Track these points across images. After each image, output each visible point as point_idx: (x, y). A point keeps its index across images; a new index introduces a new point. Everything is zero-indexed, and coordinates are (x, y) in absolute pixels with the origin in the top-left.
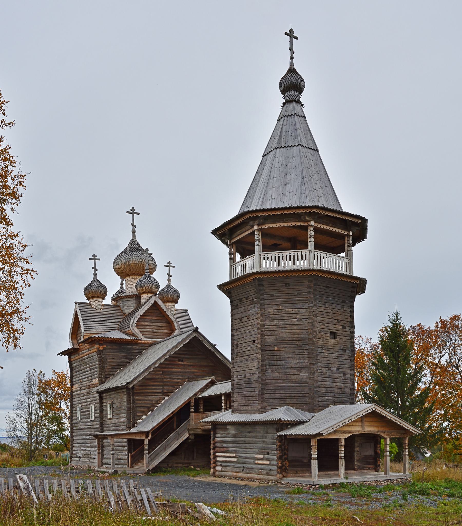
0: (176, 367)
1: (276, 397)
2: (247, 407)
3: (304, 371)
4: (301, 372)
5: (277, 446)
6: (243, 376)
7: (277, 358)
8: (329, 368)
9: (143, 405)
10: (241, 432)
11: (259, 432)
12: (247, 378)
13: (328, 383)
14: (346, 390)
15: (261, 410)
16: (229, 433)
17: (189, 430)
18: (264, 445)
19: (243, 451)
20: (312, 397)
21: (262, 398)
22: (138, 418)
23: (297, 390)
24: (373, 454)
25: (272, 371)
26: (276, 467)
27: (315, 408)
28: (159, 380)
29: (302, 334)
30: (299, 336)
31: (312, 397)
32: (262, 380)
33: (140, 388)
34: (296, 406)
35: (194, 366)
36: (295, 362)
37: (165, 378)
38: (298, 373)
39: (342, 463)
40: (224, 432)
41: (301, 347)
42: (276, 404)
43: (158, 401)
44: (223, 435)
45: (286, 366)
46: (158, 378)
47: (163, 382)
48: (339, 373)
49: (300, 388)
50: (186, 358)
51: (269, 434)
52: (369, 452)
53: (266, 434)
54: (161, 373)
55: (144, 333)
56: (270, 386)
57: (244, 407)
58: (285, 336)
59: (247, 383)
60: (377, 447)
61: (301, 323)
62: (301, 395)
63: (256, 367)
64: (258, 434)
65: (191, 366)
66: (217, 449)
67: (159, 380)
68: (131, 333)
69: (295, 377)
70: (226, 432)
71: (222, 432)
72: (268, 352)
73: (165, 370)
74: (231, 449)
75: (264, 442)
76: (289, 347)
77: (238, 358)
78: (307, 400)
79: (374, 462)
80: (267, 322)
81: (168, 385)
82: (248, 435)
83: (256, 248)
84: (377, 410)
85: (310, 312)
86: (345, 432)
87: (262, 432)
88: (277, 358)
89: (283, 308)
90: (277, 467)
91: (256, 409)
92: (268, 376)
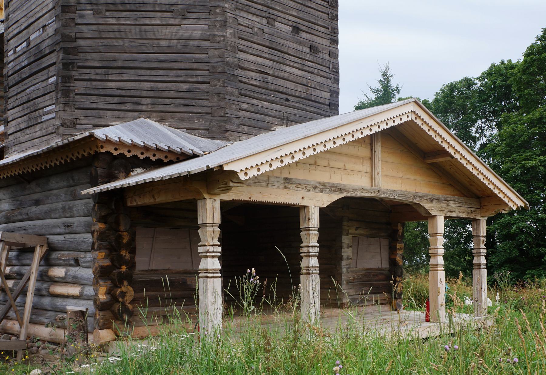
1: (108, 92)
2: (32, 130)
3: (195, 16)
4: (184, 18)
6: (24, 45)
8: (271, 20)
10: (22, 205)
12: (32, 45)
13: (269, 63)
14: (318, 93)
15: (61, 130)
20: (218, 94)
21: (66, 93)
24: (386, 265)
25: (96, 13)
27: (228, 127)
31: (218, 94)
32: (65, 38)
34: (173, 119)
38: (177, 21)
39: (311, 286)
42: (109, 113)
48: (300, 43)
49: (182, 65)
52: (375, 259)
56: (89, 56)
57: (28, 131)
59: (32, 59)
60: (396, 249)
62: (185, 87)
64: (53, 206)
78: (205, 103)
79: (384, 287)
82: (34, 210)
84: (418, 122)
86: (321, 187)
90: (95, 302)
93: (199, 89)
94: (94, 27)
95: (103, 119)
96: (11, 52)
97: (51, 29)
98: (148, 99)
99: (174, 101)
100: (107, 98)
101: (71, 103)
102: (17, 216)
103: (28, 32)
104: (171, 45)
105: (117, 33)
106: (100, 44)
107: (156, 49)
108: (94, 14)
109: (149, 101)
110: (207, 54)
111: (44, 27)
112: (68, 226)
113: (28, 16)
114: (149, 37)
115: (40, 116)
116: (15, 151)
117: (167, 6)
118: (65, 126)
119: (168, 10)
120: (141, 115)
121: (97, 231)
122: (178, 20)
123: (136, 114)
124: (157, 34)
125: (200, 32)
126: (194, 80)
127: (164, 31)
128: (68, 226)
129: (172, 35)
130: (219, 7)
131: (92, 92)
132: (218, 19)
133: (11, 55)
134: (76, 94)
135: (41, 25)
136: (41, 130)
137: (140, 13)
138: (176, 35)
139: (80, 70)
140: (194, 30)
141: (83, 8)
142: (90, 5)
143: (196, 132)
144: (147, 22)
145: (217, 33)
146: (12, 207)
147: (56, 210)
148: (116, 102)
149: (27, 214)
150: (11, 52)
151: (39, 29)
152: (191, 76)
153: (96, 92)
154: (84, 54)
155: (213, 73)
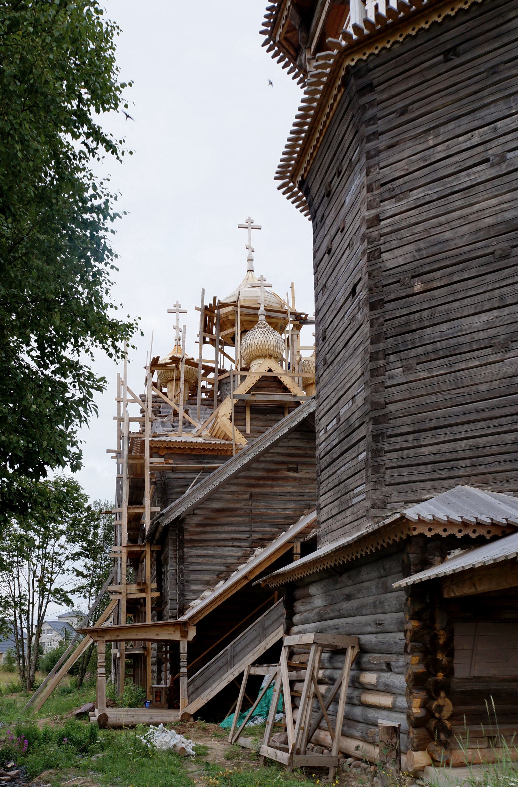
0: (280, 482)
1: (421, 460)
7: (421, 320)
9: (205, 567)
15: (372, 512)
21: (376, 469)
22: (193, 597)
25: (407, 369)
26: (404, 717)
30: (499, 218)
32: (376, 406)
34: (496, 481)
36: (484, 317)
38: (499, 357)
42: (422, 485)
43: (239, 558)
45: (452, 342)
47: (251, 515)
50: (304, 464)
54: (247, 496)
56: (399, 422)
58: (448, 235)
61: (504, 168)
70: (308, 607)
73: (257, 490)
76: (462, 270)
80: (390, 207)
82: (346, 605)
88: (421, 320)
89: (440, 139)
90: (409, 717)
95: (415, 494)
98: (466, 461)
100: (420, 467)
101: (381, 479)
106: (412, 405)
107: (474, 397)
109: (467, 462)
117: (487, 341)
122: (499, 355)
123: (452, 481)
129: (493, 375)
131: (404, 463)
134: (387, 469)
138: (497, 374)
141: (393, 368)
142: (400, 362)
144: (463, 366)
153: (408, 462)
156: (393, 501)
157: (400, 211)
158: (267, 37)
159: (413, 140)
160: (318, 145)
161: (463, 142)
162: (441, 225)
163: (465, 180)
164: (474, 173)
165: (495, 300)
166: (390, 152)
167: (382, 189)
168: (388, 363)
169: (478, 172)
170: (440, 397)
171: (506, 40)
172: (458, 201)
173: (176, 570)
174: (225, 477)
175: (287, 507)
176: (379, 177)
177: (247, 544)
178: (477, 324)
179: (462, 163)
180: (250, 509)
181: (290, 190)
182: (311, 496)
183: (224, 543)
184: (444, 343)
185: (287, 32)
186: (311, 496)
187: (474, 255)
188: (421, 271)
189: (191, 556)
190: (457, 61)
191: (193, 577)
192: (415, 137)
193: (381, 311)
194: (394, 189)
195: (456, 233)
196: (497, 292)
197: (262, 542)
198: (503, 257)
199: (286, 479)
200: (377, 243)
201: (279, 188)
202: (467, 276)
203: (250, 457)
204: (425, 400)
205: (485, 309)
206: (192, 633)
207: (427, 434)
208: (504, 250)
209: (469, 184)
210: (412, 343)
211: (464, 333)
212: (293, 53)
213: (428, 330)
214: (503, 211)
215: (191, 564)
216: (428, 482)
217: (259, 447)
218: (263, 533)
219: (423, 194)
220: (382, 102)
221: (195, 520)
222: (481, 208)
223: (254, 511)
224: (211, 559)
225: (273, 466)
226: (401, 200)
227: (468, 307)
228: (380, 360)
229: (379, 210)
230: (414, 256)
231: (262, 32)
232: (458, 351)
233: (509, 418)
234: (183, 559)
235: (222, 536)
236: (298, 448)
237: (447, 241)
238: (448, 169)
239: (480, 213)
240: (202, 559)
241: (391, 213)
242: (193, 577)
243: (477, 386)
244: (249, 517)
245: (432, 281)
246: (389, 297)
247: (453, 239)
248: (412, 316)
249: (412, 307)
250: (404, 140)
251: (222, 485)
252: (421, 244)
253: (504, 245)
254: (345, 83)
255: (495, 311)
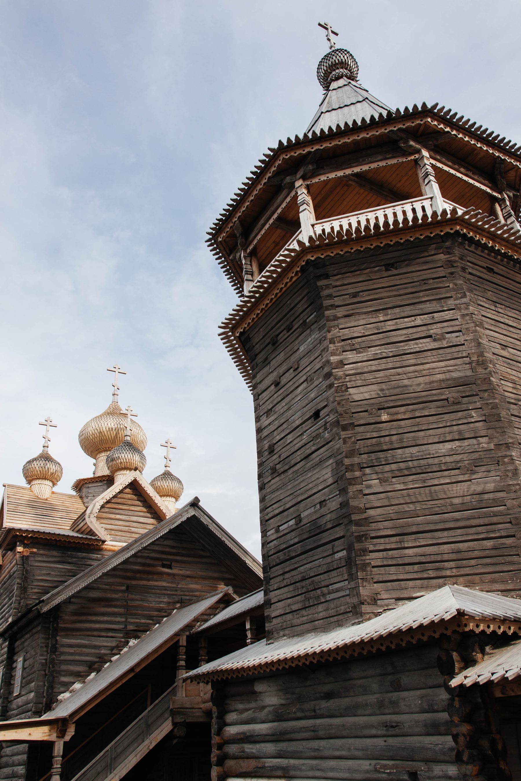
0: (155, 577)
1: (407, 560)
2: (312, 610)
3: (483, 469)
4: (473, 472)
5: (455, 738)
7: (391, 443)
9: (77, 658)
11: (366, 691)
12: (304, 522)
16: (264, 707)
17: (173, 713)
18: (391, 741)
19: (312, 768)
22: (62, 689)
23: (473, 530)
25: (382, 481)
28: (118, 603)
29: (456, 370)
30: (448, 376)
33: (75, 618)
34: (482, 582)
35: (195, 578)
36: (448, 446)
37: (133, 600)
38: (466, 477)
40: (247, 706)
41: (459, 403)
42: (411, 583)
43: (112, 649)
44: (245, 716)
46: (117, 600)
47: (126, 607)
51: (405, 694)
53: (395, 695)
54: (124, 588)
55: (113, 532)
56: (380, 525)
57: (304, 612)
58: (406, 382)
59: (305, 536)
62: (489, 544)
63: (330, 481)
64: (361, 699)
65: (188, 576)
66: (230, 763)
67: (118, 603)
68: (88, 530)
69: (460, 491)
70: (253, 705)
71: (241, 706)
72: (361, 429)
73: (134, 582)
74: (270, 762)
75: (392, 729)
76: (423, 409)
77: (277, 479)
81: (139, 615)
82: (324, 704)
83: (303, 217)
85: (463, 316)
87: (375, 687)
89: (389, 317)
91: (343, 609)
92: (372, 497)
93: (504, 544)
94: (382, 496)
95: (405, 591)
96: (273, 531)
97: (334, 503)
98: (451, 563)
99: (480, 561)
100: (407, 567)
101: (368, 577)
102: (295, 713)
103: (298, 510)
104: (465, 501)
105: (401, 499)
106: (391, 512)
107: (450, 509)
108: (380, 483)
109: (452, 564)
110: (505, 505)
111: (322, 503)
112: (392, 727)
113: (294, 494)
114: (440, 497)
115: (324, 595)
116: (284, 636)
117: (453, 464)
118: (365, 603)
119: (455, 467)
120: (446, 582)
121: (464, 735)
122: (466, 476)
123: (441, 581)
124: (448, 493)
125: (493, 485)
126: (497, 535)
127: (454, 489)
128: (392, 727)
129: (464, 492)
130: (506, 456)
131: (390, 563)
132: (508, 468)
133: (272, 534)
134: (373, 567)
135: (318, 501)
136: (327, 610)
137: (427, 475)
138: (468, 491)
139: (374, 540)
140: (486, 483)
141: (369, 479)
142: (375, 475)
143: (513, 593)
144: (436, 482)
145: (511, 483)
146: (283, 702)
147: (367, 705)
148: (417, 570)
149: (314, 711)
150: (273, 531)
151: (315, 505)
152: (493, 531)
153: (394, 562)
154: (375, 524)
155: (516, 525)
156: (384, 598)
157: (361, 360)
158: (211, 237)
159: (367, 315)
160: (266, 309)
161: (407, 322)
162: (399, 375)
163: (413, 346)
164: (421, 343)
165: (455, 433)
166: (347, 319)
167: (343, 343)
168: (364, 475)
169: (424, 343)
170: (418, 506)
171: (431, 266)
172: (411, 360)
173: (46, 660)
174: (108, 569)
175: (161, 600)
176: (340, 334)
177: (121, 635)
178: (443, 451)
179: (410, 336)
180: (126, 601)
181: (228, 337)
182: (183, 591)
183: (99, 633)
184: (415, 463)
185: (227, 237)
186: (183, 591)
187: (431, 399)
188: (386, 406)
189: (63, 646)
190: (395, 272)
191: (64, 667)
192: (365, 313)
193: (352, 432)
194: (354, 345)
195: (413, 381)
196: (455, 428)
197: (138, 632)
198: (454, 403)
199: (162, 574)
200: (343, 380)
201: (219, 335)
202: (427, 414)
203: (133, 552)
204: (404, 508)
205: (447, 439)
206: (71, 732)
207: (409, 537)
208: (456, 399)
209: (418, 350)
210: (385, 460)
211: (432, 456)
212: (228, 251)
213: (400, 451)
214: (449, 371)
215: (63, 653)
216: (417, 581)
217: (141, 543)
218: (137, 624)
219: (380, 351)
220: (336, 286)
221: (71, 608)
222: (431, 367)
223: (130, 603)
224: (84, 650)
225: (148, 561)
226: (360, 353)
227: (432, 437)
228: (356, 471)
229: (342, 357)
230: (378, 394)
231: (208, 233)
232: (429, 470)
233: (484, 527)
234: (56, 648)
235: (97, 626)
236: (173, 547)
237: (406, 386)
238: (399, 337)
239: (431, 371)
240: (75, 649)
241: (354, 361)
242: (64, 667)
243: (451, 499)
244: (124, 608)
245: (397, 414)
246: (359, 422)
247: (411, 386)
248: (382, 439)
249: (381, 432)
250: (359, 314)
251: (104, 574)
252: (384, 386)
253: (455, 395)
254: (303, 270)
255: (456, 442)
